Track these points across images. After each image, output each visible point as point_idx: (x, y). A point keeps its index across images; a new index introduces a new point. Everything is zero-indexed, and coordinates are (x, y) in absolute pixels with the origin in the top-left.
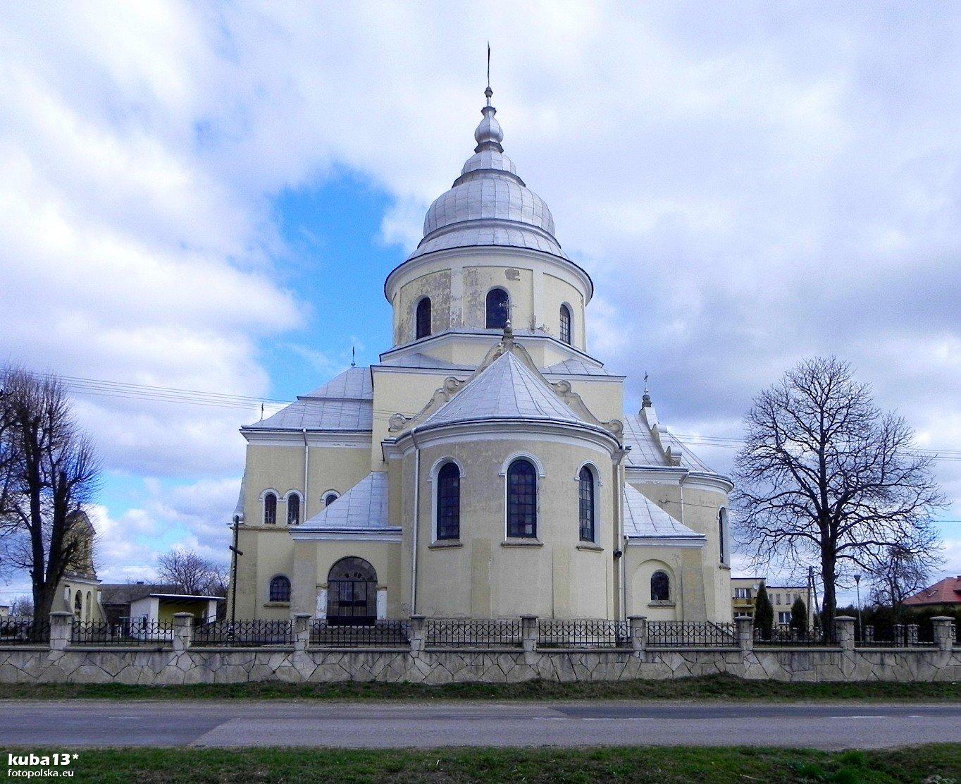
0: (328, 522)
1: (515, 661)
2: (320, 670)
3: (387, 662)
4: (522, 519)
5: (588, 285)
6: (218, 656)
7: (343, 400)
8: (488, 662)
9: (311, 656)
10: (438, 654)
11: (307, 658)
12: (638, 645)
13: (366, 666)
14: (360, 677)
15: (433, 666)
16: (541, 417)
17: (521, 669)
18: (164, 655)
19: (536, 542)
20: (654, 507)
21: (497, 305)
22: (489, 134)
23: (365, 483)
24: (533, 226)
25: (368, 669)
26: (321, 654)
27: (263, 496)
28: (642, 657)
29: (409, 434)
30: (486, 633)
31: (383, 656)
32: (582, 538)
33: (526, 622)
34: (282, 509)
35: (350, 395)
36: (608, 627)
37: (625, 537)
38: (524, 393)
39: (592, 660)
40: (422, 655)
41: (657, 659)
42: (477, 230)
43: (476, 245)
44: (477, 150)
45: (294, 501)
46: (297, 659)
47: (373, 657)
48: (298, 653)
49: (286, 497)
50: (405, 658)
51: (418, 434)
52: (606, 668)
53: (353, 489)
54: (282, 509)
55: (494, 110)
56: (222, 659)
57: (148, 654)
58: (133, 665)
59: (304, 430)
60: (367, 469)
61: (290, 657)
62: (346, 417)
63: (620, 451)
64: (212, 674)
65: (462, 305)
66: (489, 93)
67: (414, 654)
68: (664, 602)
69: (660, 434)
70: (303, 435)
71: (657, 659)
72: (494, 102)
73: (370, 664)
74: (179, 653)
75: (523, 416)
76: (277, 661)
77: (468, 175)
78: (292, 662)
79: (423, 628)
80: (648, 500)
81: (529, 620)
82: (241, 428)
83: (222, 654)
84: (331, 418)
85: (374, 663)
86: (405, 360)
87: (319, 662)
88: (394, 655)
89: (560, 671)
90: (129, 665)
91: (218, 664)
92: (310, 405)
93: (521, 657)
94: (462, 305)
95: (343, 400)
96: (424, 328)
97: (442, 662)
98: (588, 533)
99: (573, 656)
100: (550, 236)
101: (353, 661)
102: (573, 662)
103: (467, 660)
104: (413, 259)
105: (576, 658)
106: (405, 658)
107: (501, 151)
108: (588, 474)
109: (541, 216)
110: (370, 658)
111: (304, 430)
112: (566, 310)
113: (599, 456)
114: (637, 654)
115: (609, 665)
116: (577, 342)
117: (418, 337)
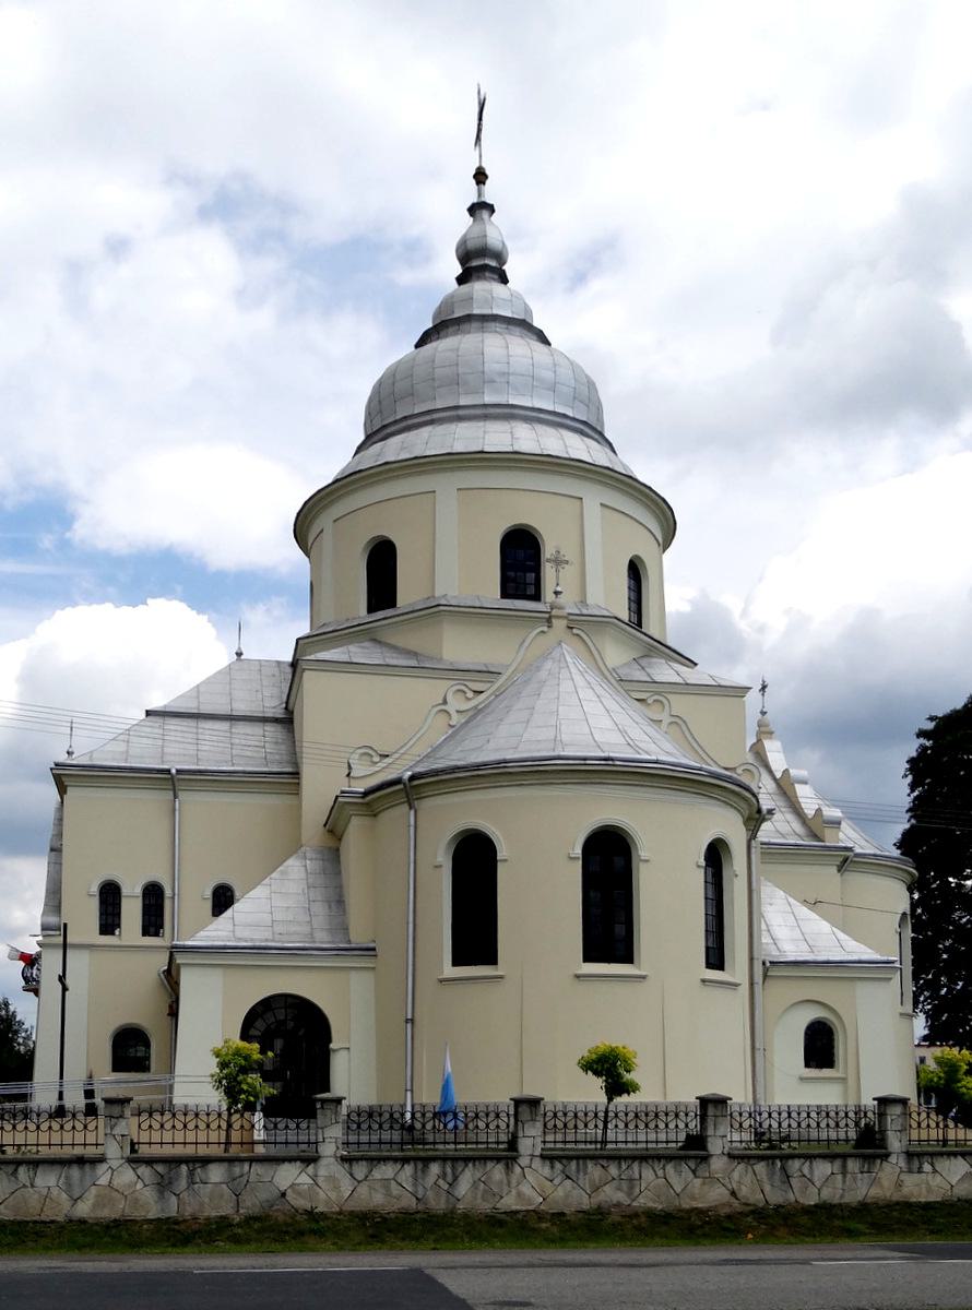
0: (238, 934)
1: (694, 1172)
2: (363, 1190)
3: (478, 1175)
4: (609, 929)
5: (668, 525)
6: (184, 1168)
7: (231, 718)
8: (648, 1174)
9: (346, 1166)
10: (564, 1161)
11: (340, 1171)
12: (895, 1143)
13: (441, 1182)
14: (438, 1204)
15: (556, 1182)
16: (638, 756)
17: (704, 1184)
18: (87, 1166)
19: (637, 972)
20: (804, 911)
21: (521, 558)
22: (484, 251)
23: (294, 866)
24: (574, 419)
25: (446, 1187)
26: (364, 1163)
27: (95, 889)
28: (902, 1164)
29: (398, 781)
30: (832, 1124)
31: (470, 1165)
32: (709, 965)
33: (524, 1109)
34: (132, 911)
35: (241, 708)
36: (650, 1126)
37: (764, 963)
38: (580, 710)
39: (823, 1169)
40: (537, 1163)
41: (927, 1167)
42: (481, 424)
43: (482, 452)
44: (461, 280)
45: (154, 897)
46: (322, 1172)
47: (453, 1168)
48: (323, 1162)
49: (138, 891)
50: (509, 1169)
51: (415, 783)
52: (844, 1182)
53: (273, 875)
54: (132, 911)
55: (491, 209)
56: (191, 1173)
57: (57, 1168)
58: (32, 1186)
59: (174, 771)
60: (294, 847)
61: (310, 1169)
62: (252, 749)
63: (757, 816)
64: (174, 1198)
65: (453, 559)
66: (480, 177)
67: (524, 1161)
68: (826, 1072)
69: (798, 787)
70: (169, 781)
71: (927, 1167)
72: (490, 193)
73: (450, 1178)
74: (115, 1164)
75: (612, 755)
76: (288, 1176)
77: (442, 327)
78: (314, 1178)
79: (538, 1118)
80: (791, 900)
81: (528, 1106)
82: (53, 766)
83: (191, 1165)
84: (211, 749)
85: (456, 1178)
86: (356, 652)
87: (360, 1176)
88: (490, 1165)
89: (767, 1188)
90: (24, 1186)
91: (183, 1183)
92: (173, 724)
93: (703, 1166)
94: (453, 559)
95: (231, 718)
96: (382, 590)
97: (573, 1174)
98: (716, 958)
99: (790, 1162)
100: (591, 430)
101: (419, 1173)
102: (790, 1172)
103: (613, 1170)
104: (360, 471)
105: (795, 1165)
106: (509, 1169)
107: (504, 280)
108: (716, 854)
109: (587, 401)
110: (449, 1170)
111: (174, 771)
112: (635, 571)
113: (725, 823)
114: (893, 1159)
115: (849, 1176)
116: (651, 625)
117: (371, 609)
